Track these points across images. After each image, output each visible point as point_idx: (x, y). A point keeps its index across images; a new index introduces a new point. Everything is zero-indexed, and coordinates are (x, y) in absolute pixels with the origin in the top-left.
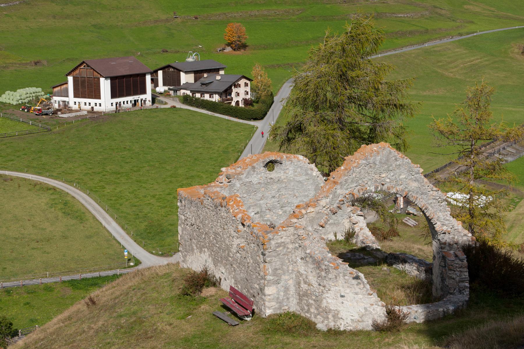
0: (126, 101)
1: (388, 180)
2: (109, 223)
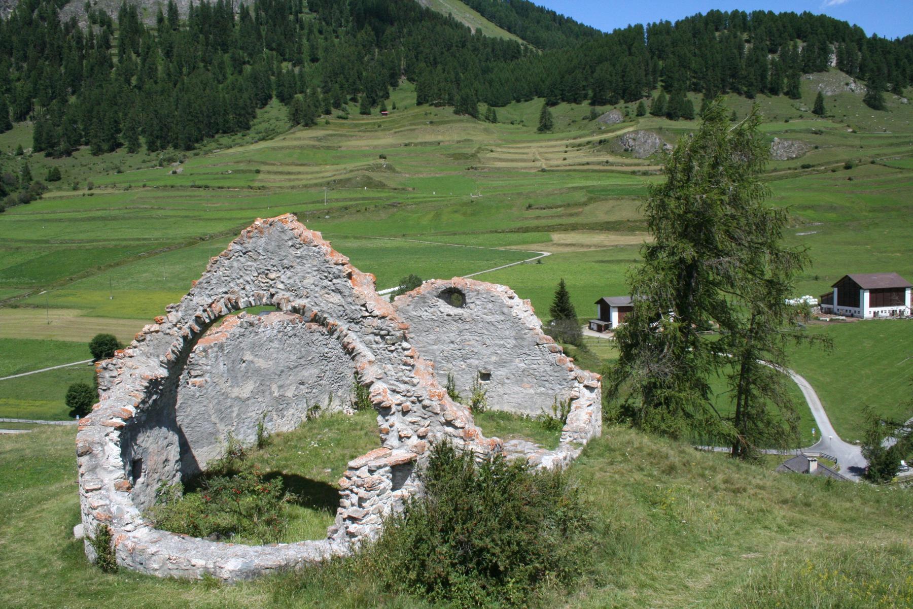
0: (885, 311)
1: (281, 286)
2: (817, 410)
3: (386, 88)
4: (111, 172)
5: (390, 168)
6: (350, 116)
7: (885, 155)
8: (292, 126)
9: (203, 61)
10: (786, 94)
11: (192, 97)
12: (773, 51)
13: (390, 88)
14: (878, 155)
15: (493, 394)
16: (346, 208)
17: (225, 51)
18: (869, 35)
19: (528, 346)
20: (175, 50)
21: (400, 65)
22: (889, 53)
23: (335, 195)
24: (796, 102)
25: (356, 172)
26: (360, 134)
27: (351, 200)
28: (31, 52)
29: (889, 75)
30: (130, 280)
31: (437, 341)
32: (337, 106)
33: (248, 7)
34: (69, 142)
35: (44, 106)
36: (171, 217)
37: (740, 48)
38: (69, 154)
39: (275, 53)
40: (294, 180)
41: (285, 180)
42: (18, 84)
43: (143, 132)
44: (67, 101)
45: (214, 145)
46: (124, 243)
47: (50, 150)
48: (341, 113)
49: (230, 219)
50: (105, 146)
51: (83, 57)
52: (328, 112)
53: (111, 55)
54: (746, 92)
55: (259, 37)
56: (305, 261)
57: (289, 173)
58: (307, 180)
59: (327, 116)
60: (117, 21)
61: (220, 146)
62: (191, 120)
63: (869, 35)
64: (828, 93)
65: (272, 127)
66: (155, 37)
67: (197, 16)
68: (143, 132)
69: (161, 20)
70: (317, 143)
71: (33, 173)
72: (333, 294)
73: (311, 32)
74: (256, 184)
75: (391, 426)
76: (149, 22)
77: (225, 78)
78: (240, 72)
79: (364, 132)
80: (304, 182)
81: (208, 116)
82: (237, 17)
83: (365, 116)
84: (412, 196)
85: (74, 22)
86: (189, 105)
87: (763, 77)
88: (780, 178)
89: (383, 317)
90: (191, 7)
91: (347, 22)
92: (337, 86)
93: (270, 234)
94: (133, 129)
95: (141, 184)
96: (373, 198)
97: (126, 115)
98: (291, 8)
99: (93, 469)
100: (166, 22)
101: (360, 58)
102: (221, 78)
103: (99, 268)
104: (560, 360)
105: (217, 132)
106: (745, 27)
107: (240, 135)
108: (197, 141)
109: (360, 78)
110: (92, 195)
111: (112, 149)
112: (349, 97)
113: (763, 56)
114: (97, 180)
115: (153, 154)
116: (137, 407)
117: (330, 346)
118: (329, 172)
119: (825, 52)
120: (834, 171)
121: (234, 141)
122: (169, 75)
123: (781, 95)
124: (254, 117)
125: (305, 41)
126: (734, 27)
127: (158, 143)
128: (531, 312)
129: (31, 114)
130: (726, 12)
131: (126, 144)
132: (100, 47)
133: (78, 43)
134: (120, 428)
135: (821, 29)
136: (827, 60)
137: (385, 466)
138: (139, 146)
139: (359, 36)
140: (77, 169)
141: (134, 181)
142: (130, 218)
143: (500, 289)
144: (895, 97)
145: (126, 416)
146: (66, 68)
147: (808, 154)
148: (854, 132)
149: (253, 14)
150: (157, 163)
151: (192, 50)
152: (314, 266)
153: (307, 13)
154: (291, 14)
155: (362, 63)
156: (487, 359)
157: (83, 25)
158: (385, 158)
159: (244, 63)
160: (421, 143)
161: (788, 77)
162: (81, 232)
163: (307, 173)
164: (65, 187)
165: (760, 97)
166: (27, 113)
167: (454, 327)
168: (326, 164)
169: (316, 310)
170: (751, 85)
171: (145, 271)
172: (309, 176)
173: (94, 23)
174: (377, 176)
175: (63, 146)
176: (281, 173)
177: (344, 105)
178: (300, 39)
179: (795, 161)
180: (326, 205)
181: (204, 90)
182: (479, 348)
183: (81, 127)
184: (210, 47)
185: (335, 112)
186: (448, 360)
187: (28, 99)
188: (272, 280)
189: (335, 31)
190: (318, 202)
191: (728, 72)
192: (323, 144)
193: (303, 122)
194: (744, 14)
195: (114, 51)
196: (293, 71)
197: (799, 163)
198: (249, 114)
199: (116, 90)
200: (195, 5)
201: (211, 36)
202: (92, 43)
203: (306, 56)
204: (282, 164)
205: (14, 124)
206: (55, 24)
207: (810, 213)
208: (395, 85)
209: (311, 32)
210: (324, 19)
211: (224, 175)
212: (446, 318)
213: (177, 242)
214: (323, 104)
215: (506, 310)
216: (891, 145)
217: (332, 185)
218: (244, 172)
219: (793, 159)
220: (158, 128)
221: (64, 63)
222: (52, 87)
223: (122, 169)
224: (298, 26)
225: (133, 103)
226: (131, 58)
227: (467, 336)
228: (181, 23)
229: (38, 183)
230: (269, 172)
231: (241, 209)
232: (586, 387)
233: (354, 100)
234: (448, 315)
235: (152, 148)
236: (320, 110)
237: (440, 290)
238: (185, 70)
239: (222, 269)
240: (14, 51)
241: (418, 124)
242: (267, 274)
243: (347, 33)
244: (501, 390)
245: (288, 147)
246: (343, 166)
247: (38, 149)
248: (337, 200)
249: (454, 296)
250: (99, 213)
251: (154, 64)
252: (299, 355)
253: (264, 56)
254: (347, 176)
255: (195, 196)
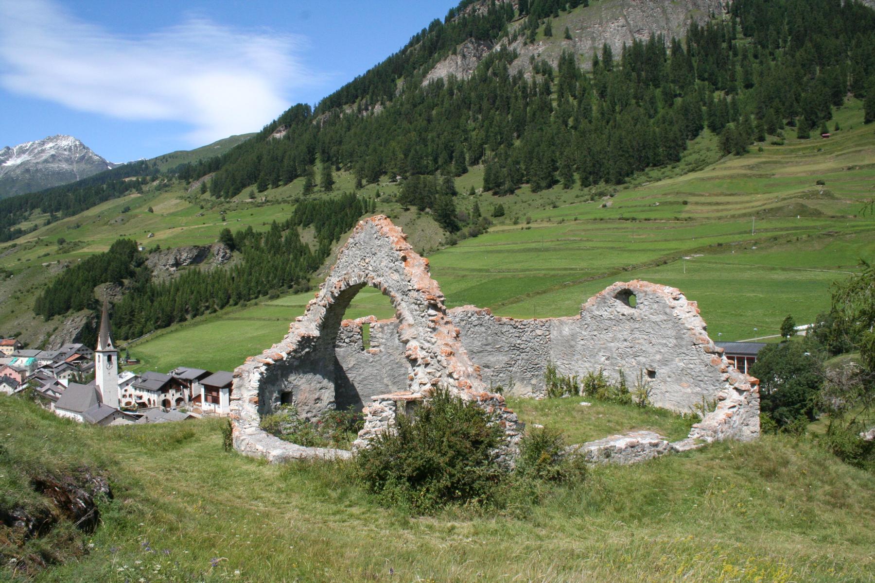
3: (828, 108)
4: (547, 207)
5: (828, 195)
6: (786, 142)
8: (723, 156)
9: (635, 97)
11: (624, 133)
13: (833, 108)
15: (657, 391)
16: (775, 239)
17: (657, 86)
19: (687, 346)
20: (608, 90)
21: (845, 82)
23: (764, 225)
25: (789, 201)
26: (797, 159)
27: (782, 229)
28: (485, 104)
30: (553, 307)
31: (614, 339)
32: (772, 131)
33: (679, 41)
34: (512, 181)
35: (493, 150)
36: (598, 248)
38: (512, 192)
39: (706, 83)
40: (722, 210)
41: (713, 211)
42: (474, 133)
43: (578, 169)
44: (512, 145)
45: (644, 178)
46: (553, 273)
47: (497, 190)
48: (775, 139)
49: (654, 250)
50: (543, 184)
51: (527, 104)
52: (761, 139)
53: (551, 100)
55: (691, 67)
57: (717, 204)
58: (736, 209)
59: (760, 144)
60: (557, 69)
61: (650, 180)
62: (622, 156)
65: (702, 158)
66: (590, 79)
67: (630, 55)
68: (578, 169)
69: (596, 63)
70: (748, 172)
71: (481, 210)
73: (745, 57)
74: (684, 216)
75: (415, 375)
76: (585, 66)
77: (656, 112)
78: (671, 105)
79: (801, 157)
80: (732, 213)
81: (638, 150)
82: (668, 52)
83: (803, 141)
84: (853, 223)
85: (521, 73)
86: (620, 141)
89: (418, 290)
90: (624, 48)
91: (785, 41)
92: (772, 110)
94: (568, 166)
95: (573, 218)
96: (807, 228)
97: (562, 154)
98: (724, 36)
99: (239, 387)
100: (601, 64)
101: (798, 79)
102: (652, 112)
103: (528, 295)
104: (713, 361)
105: (647, 166)
107: (669, 167)
108: (628, 175)
109: (797, 101)
110: (529, 228)
111: (549, 186)
112: (785, 121)
114: (533, 214)
115: (586, 190)
116: (289, 354)
117: (523, 338)
118: (759, 201)
121: (663, 173)
122: (603, 114)
124: (685, 149)
125: (738, 68)
127: (591, 179)
128: (695, 313)
129: (483, 158)
131: (562, 181)
132: (542, 94)
133: (523, 92)
134: (267, 364)
137: (390, 400)
138: (574, 182)
139: (798, 54)
140: (518, 205)
141: (567, 215)
142: (560, 250)
143: (667, 292)
145: (276, 357)
146: (512, 115)
149: (684, 47)
150: (588, 197)
151: (624, 88)
153: (742, 39)
154: (724, 41)
155: (801, 84)
156: (652, 357)
157: (528, 76)
158: (823, 184)
159: (676, 96)
160: (868, 166)
162: (517, 262)
163: (736, 203)
164: (508, 222)
166: (480, 157)
167: (628, 325)
168: (758, 193)
169: (386, 285)
171: (568, 299)
172: (738, 206)
173: (537, 73)
174: (811, 204)
175: (507, 186)
176: (710, 204)
177: (779, 131)
178: (733, 65)
180: (753, 236)
181: (635, 126)
182: (646, 347)
183: (524, 167)
184: (641, 84)
185: (769, 138)
186: (622, 357)
187: (481, 145)
189: (771, 54)
190: (745, 232)
192: (755, 172)
193: (734, 150)
195: (554, 96)
196: (725, 99)
198: (679, 146)
199: (555, 131)
200: (627, 45)
201: (643, 73)
202: (535, 91)
203: (739, 83)
204: (710, 195)
205: (469, 168)
206: (505, 78)
208: (839, 104)
209: (745, 57)
210: (760, 43)
211: (651, 207)
212: (621, 317)
213: (600, 272)
214: (756, 131)
215: (668, 310)
217: (762, 214)
218: (671, 203)
220: (591, 165)
221: (511, 111)
222: (501, 134)
223: (557, 204)
224: (731, 53)
225: (568, 142)
226: (568, 101)
227: (637, 334)
228: (615, 63)
229: (485, 219)
230: (697, 203)
231: (666, 240)
232: (736, 389)
233: (791, 124)
234: (623, 315)
235: (585, 183)
236: (753, 138)
238: (618, 108)
240: (472, 106)
241: (865, 144)
243: (785, 53)
244: (663, 388)
245: (717, 178)
246: (775, 195)
247: (487, 189)
248: (766, 230)
249: (625, 296)
250: (533, 245)
251: (589, 105)
252: (484, 342)
253: (696, 87)
254: (779, 204)
255: (622, 228)
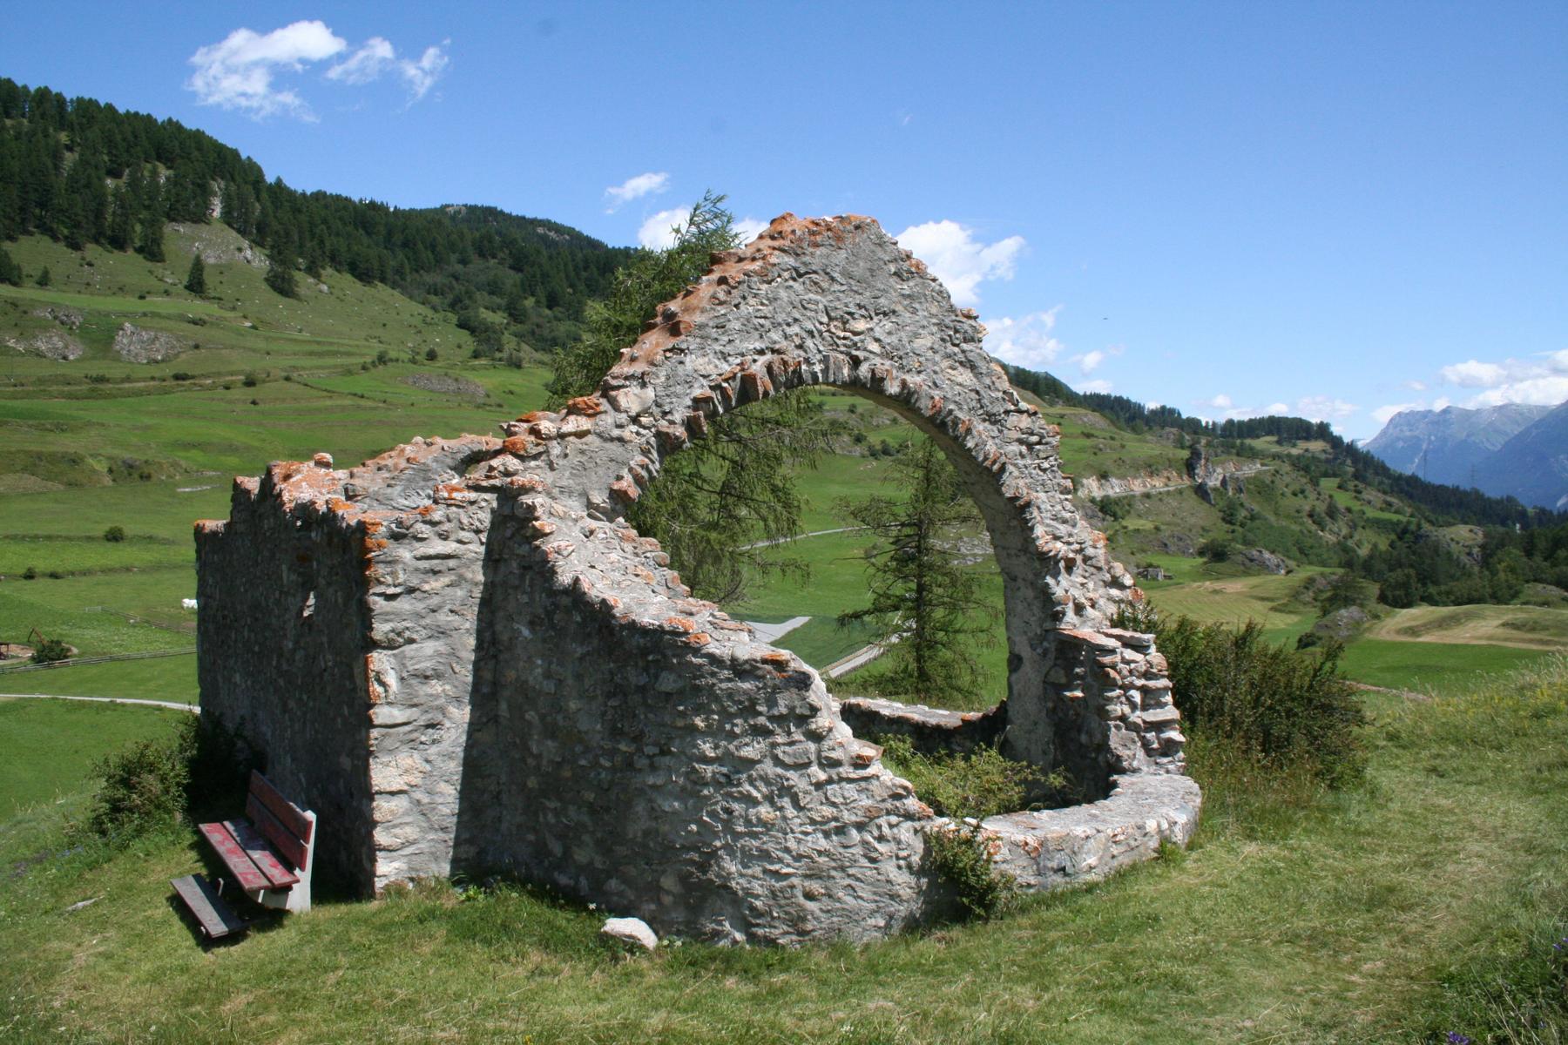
1: (875, 347)
7: (304, 368)
10: (140, 250)
12: (116, 174)
14: (295, 368)
18: (270, 178)
22: (300, 211)
24: (158, 268)
29: (301, 246)
37: (56, 157)
54: (66, 238)
56: (917, 306)
63: (270, 178)
64: (210, 259)
72: (961, 369)
87: (99, 214)
88: (138, 393)
93: (855, 244)
106: (62, 122)
113: (99, 179)
119: (204, 192)
120: (227, 388)
123: (130, 252)
126: (43, 116)
130: (25, 87)
135: (196, 153)
136: (207, 206)
144: (311, 280)
147: (183, 356)
148: (254, 327)
152: (932, 315)
161: (142, 222)
165: (92, 251)
170: (77, 225)
179: (162, 365)
188: (856, 334)
191: (33, 196)
194: (60, 99)
197: (168, 371)
207: (196, 454)
216: (311, 354)
219: (156, 362)
237: (460, 456)
239: (752, 301)
242: (845, 323)
